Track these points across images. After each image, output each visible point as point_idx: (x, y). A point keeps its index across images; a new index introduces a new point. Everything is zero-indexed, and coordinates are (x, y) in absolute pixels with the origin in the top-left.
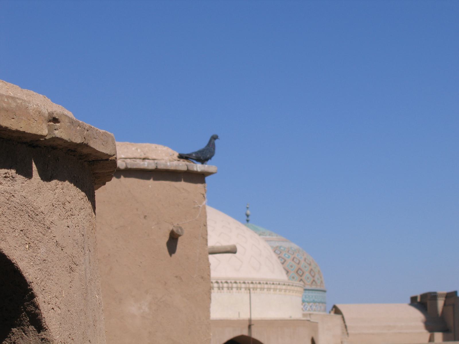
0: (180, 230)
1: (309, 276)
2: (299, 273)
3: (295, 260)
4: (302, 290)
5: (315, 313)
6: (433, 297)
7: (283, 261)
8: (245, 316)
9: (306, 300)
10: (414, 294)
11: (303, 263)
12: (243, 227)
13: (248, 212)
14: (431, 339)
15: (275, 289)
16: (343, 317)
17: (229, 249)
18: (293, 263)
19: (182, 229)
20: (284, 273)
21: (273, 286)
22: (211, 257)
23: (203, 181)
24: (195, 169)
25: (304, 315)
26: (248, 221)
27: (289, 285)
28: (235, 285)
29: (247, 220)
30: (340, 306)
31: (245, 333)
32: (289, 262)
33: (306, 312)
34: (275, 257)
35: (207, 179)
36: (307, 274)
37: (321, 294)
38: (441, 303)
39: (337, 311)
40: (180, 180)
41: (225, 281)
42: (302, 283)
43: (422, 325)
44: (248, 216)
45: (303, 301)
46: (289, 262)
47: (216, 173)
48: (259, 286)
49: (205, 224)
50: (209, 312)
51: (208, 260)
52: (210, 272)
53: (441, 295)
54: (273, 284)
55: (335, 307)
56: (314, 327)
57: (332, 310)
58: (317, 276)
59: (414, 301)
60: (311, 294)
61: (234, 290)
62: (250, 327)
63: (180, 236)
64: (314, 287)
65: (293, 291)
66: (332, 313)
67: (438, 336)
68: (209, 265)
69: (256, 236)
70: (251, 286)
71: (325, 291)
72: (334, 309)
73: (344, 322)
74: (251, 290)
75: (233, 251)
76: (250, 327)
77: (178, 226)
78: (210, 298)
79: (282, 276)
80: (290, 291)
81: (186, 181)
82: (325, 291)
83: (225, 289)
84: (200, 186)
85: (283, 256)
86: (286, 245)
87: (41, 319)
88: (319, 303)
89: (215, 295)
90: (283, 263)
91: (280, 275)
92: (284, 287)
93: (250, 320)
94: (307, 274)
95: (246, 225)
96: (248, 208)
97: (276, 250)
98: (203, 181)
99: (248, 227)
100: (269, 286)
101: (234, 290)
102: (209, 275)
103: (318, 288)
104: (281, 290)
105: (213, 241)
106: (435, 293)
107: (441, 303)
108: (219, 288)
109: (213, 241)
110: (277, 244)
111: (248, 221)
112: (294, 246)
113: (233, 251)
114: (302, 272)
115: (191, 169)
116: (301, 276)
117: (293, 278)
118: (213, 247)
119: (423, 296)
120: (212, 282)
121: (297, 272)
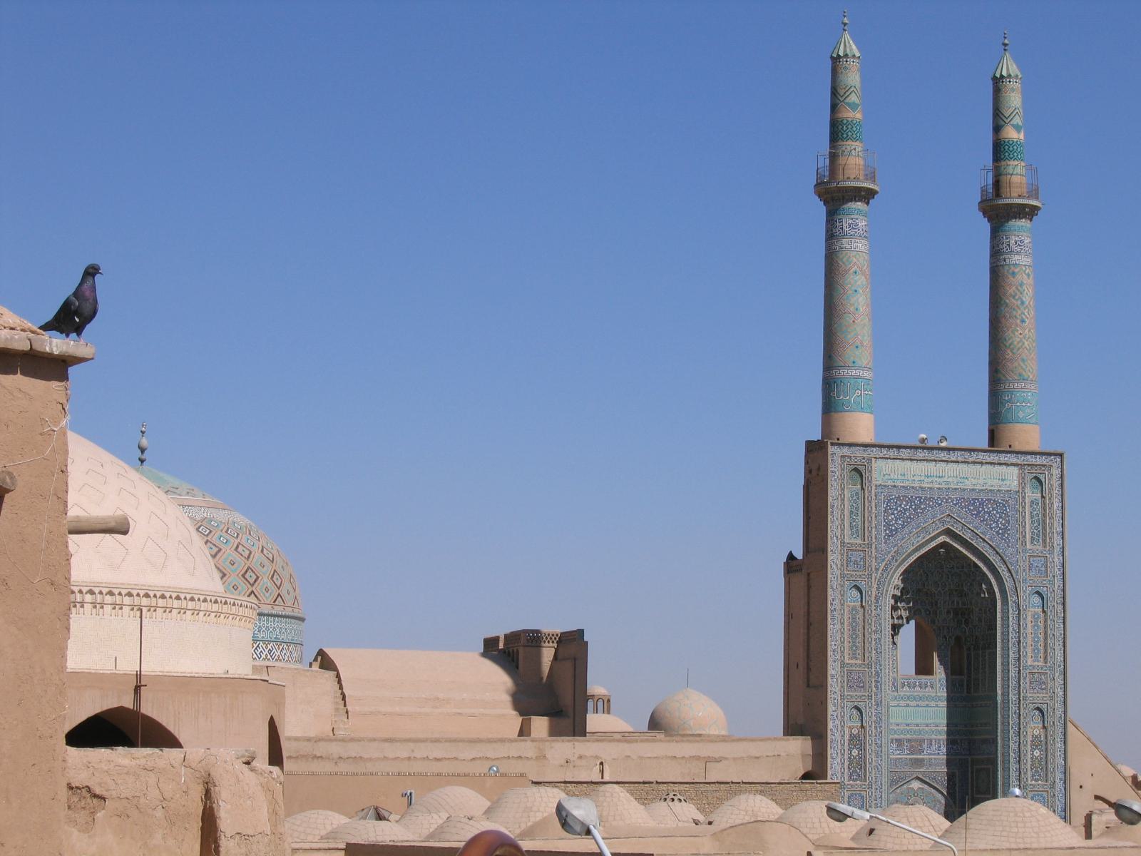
0: (8, 480)
1: (270, 585)
2: (249, 578)
3: (240, 548)
4: (255, 616)
5: (277, 664)
6: (533, 639)
7: (215, 550)
8: (128, 666)
9: (260, 636)
10: (491, 634)
11: (257, 556)
12: (134, 475)
13: (144, 442)
14: (524, 732)
15: (196, 612)
16: (338, 676)
17: (112, 524)
18: (236, 556)
19: (12, 477)
20: (217, 575)
21: (191, 605)
22: (73, 538)
23: (63, 377)
24: (48, 350)
25: (254, 668)
26: (142, 461)
27: (226, 603)
28: (108, 599)
29: (142, 458)
30: (331, 652)
31: (128, 703)
32: (228, 552)
33: (258, 663)
34: (198, 541)
35: (72, 370)
36: (265, 581)
37: (293, 625)
38: (548, 654)
39: (325, 662)
40: (15, 373)
41: (88, 588)
42: (252, 599)
43: (507, 699)
44: (143, 450)
45: (255, 640)
46: (228, 552)
47: (92, 359)
48: (161, 602)
49: (64, 469)
50: (64, 657)
51: (67, 547)
52: (69, 571)
53: (551, 637)
54: (192, 599)
55: (321, 653)
56: (276, 693)
57: (316, 660)
58: (286, 586)
59: (490, 648)
60: (272, 623)
61: (108, 608)
62: (137, 689)
63: (8, 491)
64: (278, 610)
65: (235, 616)
66: (316, 667)
67: (540, 725)
68: (68, 557)
69: (161, 494)
70: (145, 601)
71: (302, 620)
72: (319, 658)
73: (341, 687)
74: (145, 610)
75: (120, 528)
76: (137, 689)
77: (4, 469)
78: (68, 629)
79: (214, 585)
80: (227, 615)
81: (24, 373)
82: (302, 620)
83: (88, 607)
84: (55, 384)
85: (215, 540)
86: (221, 516)
87: (985, 741)
88: (288, 643)
89: (81, 622)
90: (214, 556)
91: (206, 580)
92: (215, 607)
93: (139, 676)
94: (265, 581)
95: (137, 470)
96: (143, 432)
97: (204, 528)
98: (63, 377)
99: (142, 473)
100: (183, 604)
101: (108, 608)
102: (68, 579)
103: (288, 612)
104: (208, 613)
105: (81, 504)
106: (538, 632)
107: (548, 654)
108: (94, 605)
109: (81, 504)
110: (201, 514)
111: (142, 461)
112: (240, 519)
113: (120, 528)
114: (247, 576)
115: (37, 347)
116: (252, 585)
117: (236, 588)
118: (78, 519)
119: (512, 638)
120: (73, 592)
121: (243, 576)
